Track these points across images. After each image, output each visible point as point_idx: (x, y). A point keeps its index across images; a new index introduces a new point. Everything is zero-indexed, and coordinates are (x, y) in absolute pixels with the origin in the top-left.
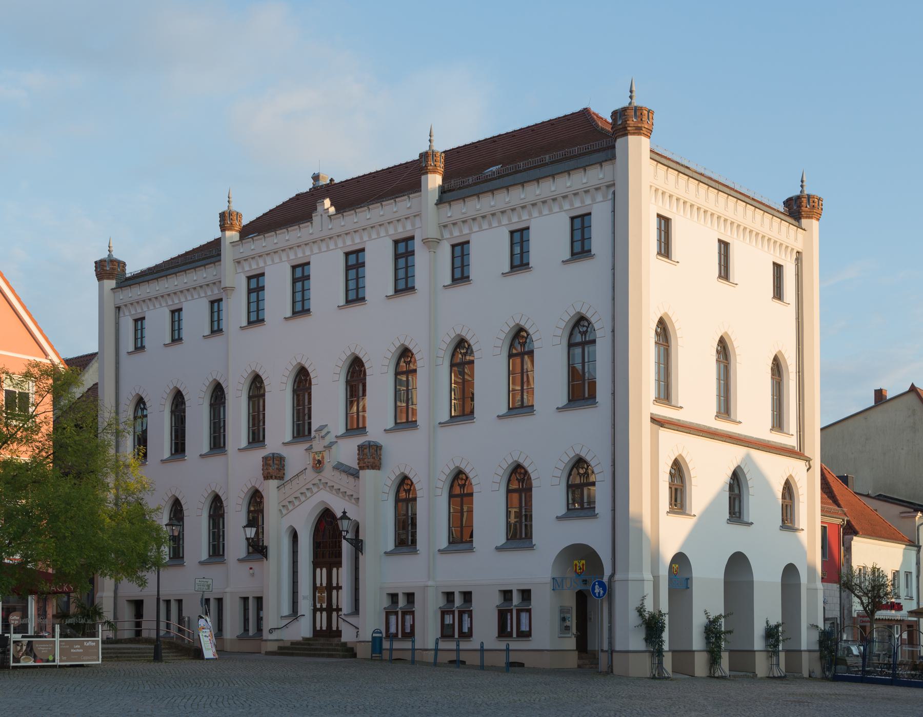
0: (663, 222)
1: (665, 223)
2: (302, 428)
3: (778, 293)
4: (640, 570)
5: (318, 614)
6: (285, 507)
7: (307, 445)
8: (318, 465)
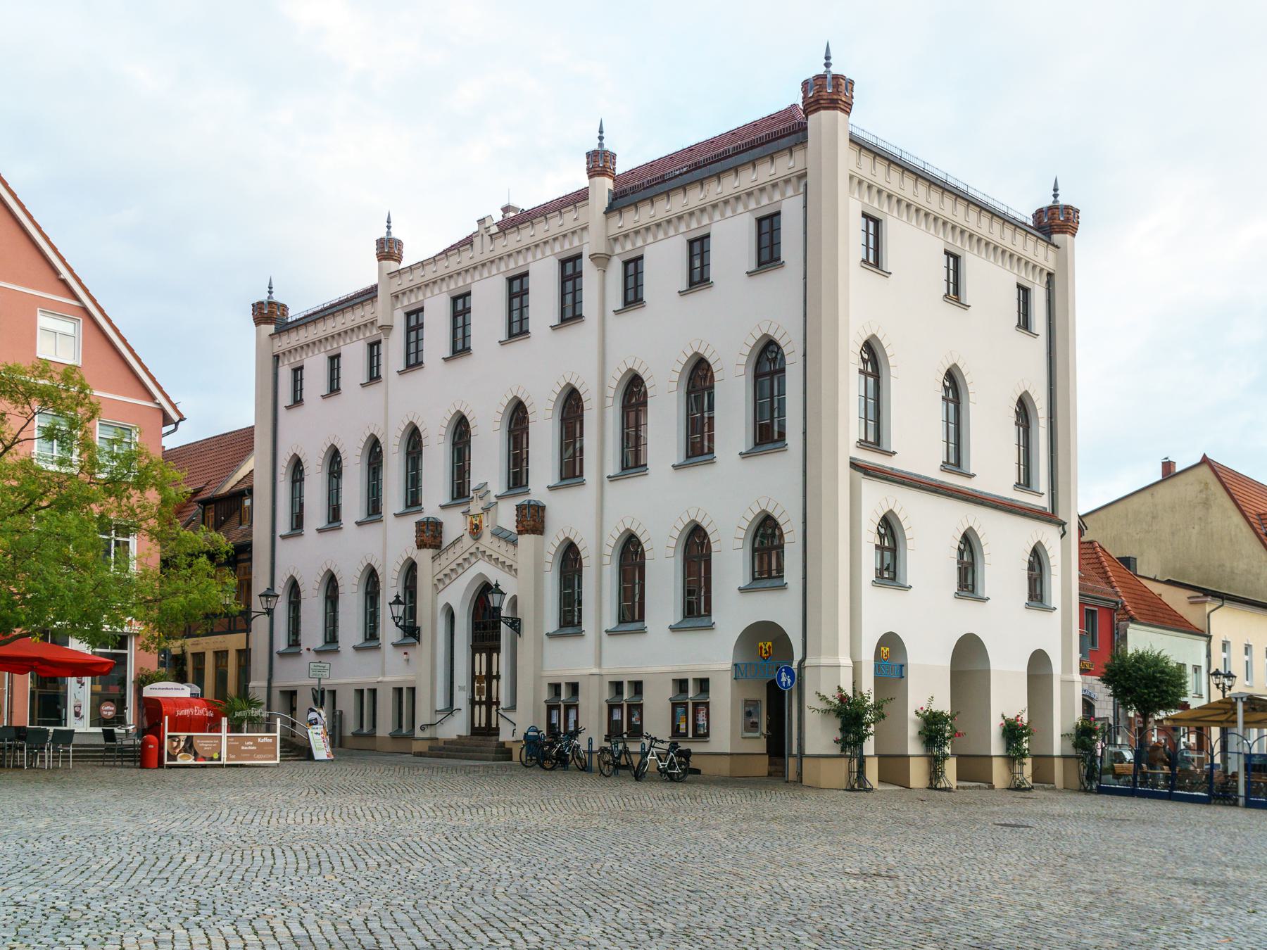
0: (871, 224)
1: (874, 223)
2: (460, 490)
3: (1025, 323)
4: (835, 652)
5: (477, 707)
6: (441, 583)
7: (464, 508)
8: (476, 531)
